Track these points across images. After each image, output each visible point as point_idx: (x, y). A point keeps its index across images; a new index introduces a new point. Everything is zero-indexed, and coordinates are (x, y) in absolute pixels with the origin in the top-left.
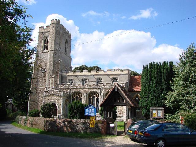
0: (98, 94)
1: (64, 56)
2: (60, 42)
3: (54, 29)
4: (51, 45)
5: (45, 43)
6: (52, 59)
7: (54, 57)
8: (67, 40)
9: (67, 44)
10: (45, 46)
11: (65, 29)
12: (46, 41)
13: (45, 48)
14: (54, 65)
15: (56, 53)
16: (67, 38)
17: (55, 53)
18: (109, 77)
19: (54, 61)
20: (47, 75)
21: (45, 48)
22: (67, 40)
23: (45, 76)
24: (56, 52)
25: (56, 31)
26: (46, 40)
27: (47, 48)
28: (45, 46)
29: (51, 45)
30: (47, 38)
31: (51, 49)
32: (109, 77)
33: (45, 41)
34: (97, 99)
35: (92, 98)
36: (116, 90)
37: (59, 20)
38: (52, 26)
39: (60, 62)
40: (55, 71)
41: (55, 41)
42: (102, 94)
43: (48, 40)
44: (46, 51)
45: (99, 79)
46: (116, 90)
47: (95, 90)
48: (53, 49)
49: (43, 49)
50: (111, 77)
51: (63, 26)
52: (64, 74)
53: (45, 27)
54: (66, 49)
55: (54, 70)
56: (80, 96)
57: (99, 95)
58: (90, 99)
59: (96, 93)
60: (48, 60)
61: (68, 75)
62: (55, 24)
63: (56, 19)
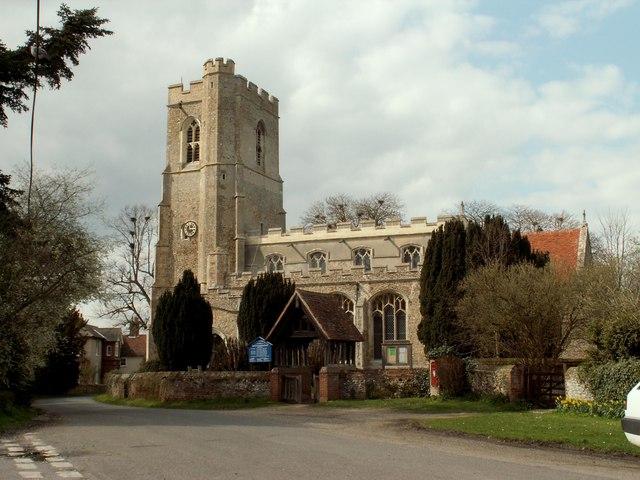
0: (349, 300)
1: (255, 179)
2: (237, 136)
3: (216, 90)
4: (207, 144)
5: (189, 140)
6: (213, 193)
7: (220, 186)
8: (261, 124)
9: (262, 137)
10: (190, 148)
11: (253, 87)
12: (192, 134)
13: (192, 155)
14: (220, 210)
15: (223, 172)
16: (258, 116)
17: (222, 174)
18: (393, 242)
19: (220, 199)
20: (201, 245)
21: (192, 155)
22: (261, 124)
23: (194, 251)
24: (223, 173)
25: (220, 98)
26: (194, 129)
27: (197, 158)
28: (190, 148)
29: (207, 144)
30: (194, 123)
31: (208, 159)
32: (393, 242)
33: (189, 132)
34: (401, 317)
35: (382, 313)
36: (297, 305)
37: (231, 63)
38: (207, 82)
39: (239, 202)
40: (225, 231)
41: (220, 132)
42: (360, 303)
43: (198, 130)
44: (193, 165)
45: (363, 251)
46: (297, 305)
47: (339, 289)
48: (214, 160)
49: (85, 343)
50: (401, 242)
51: (244, 80)
52: (254, 240)
53: (187, 88)
54: (261, 154)
55: (220, 229)
56: (397, 308)
57: (352, 305)
58: (377, 319)
59: (345, 298)
60: (202, 196)
61: (264, 240)
62: (217, 76)
63: (220, 60)
